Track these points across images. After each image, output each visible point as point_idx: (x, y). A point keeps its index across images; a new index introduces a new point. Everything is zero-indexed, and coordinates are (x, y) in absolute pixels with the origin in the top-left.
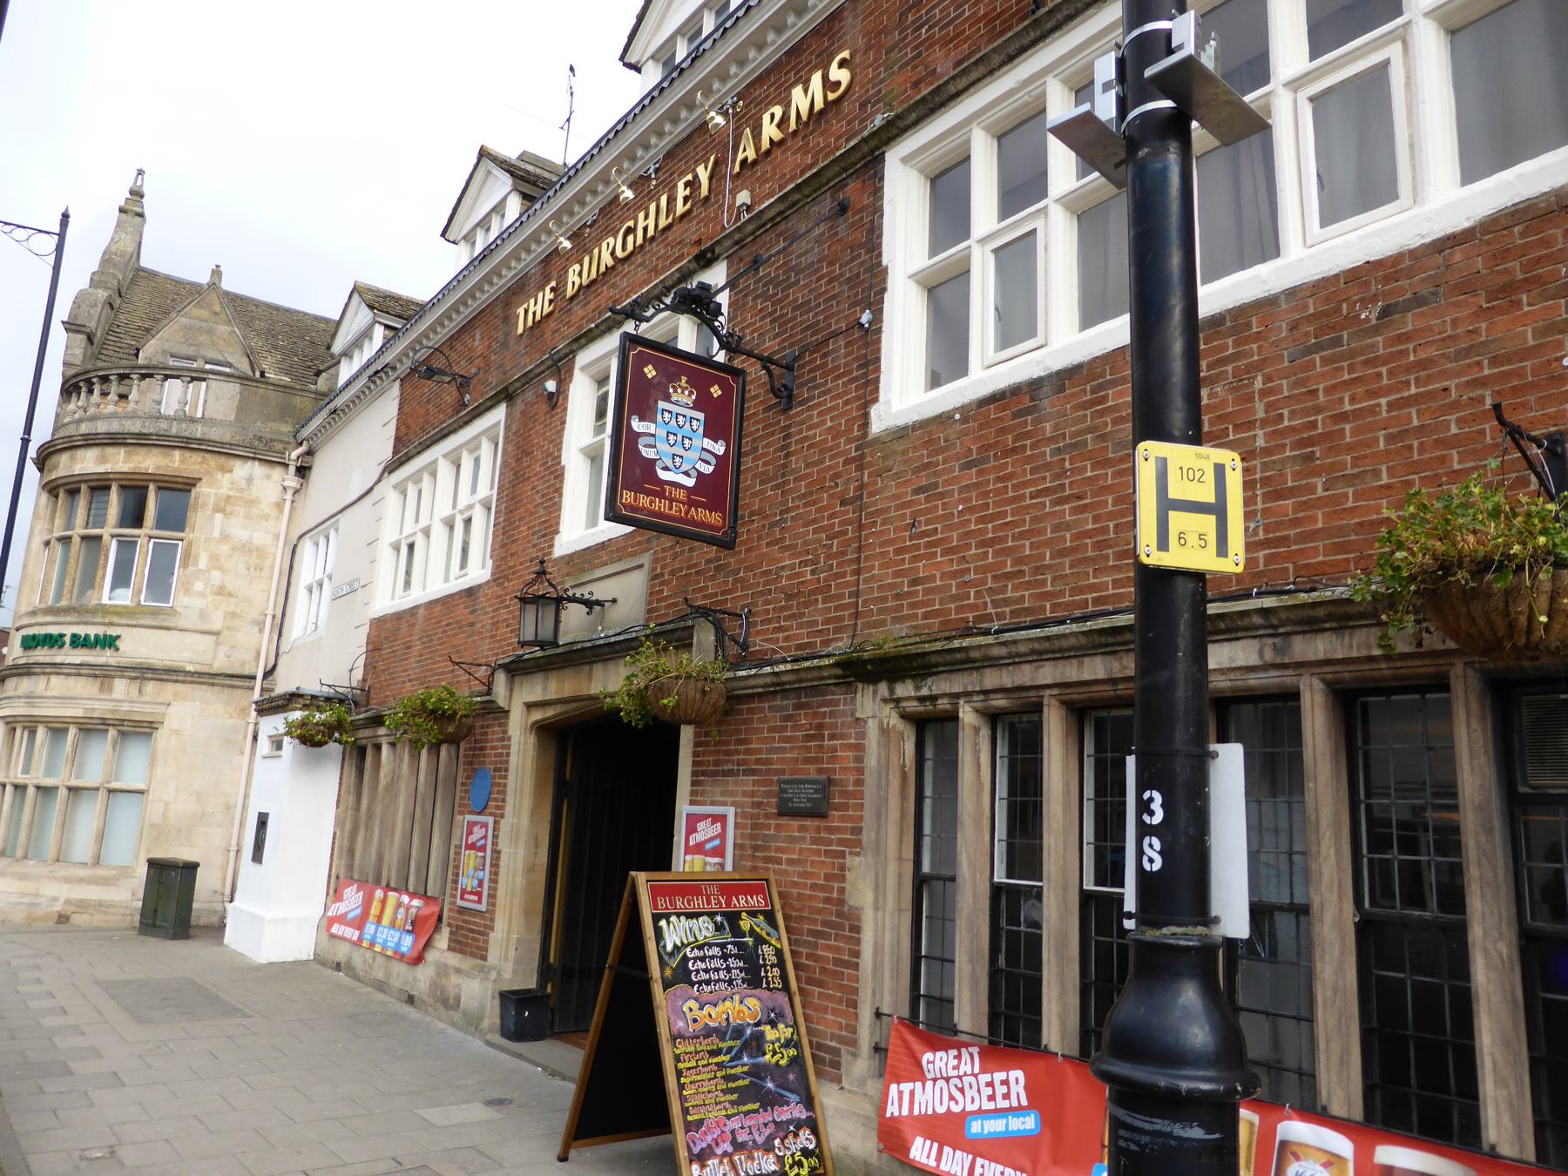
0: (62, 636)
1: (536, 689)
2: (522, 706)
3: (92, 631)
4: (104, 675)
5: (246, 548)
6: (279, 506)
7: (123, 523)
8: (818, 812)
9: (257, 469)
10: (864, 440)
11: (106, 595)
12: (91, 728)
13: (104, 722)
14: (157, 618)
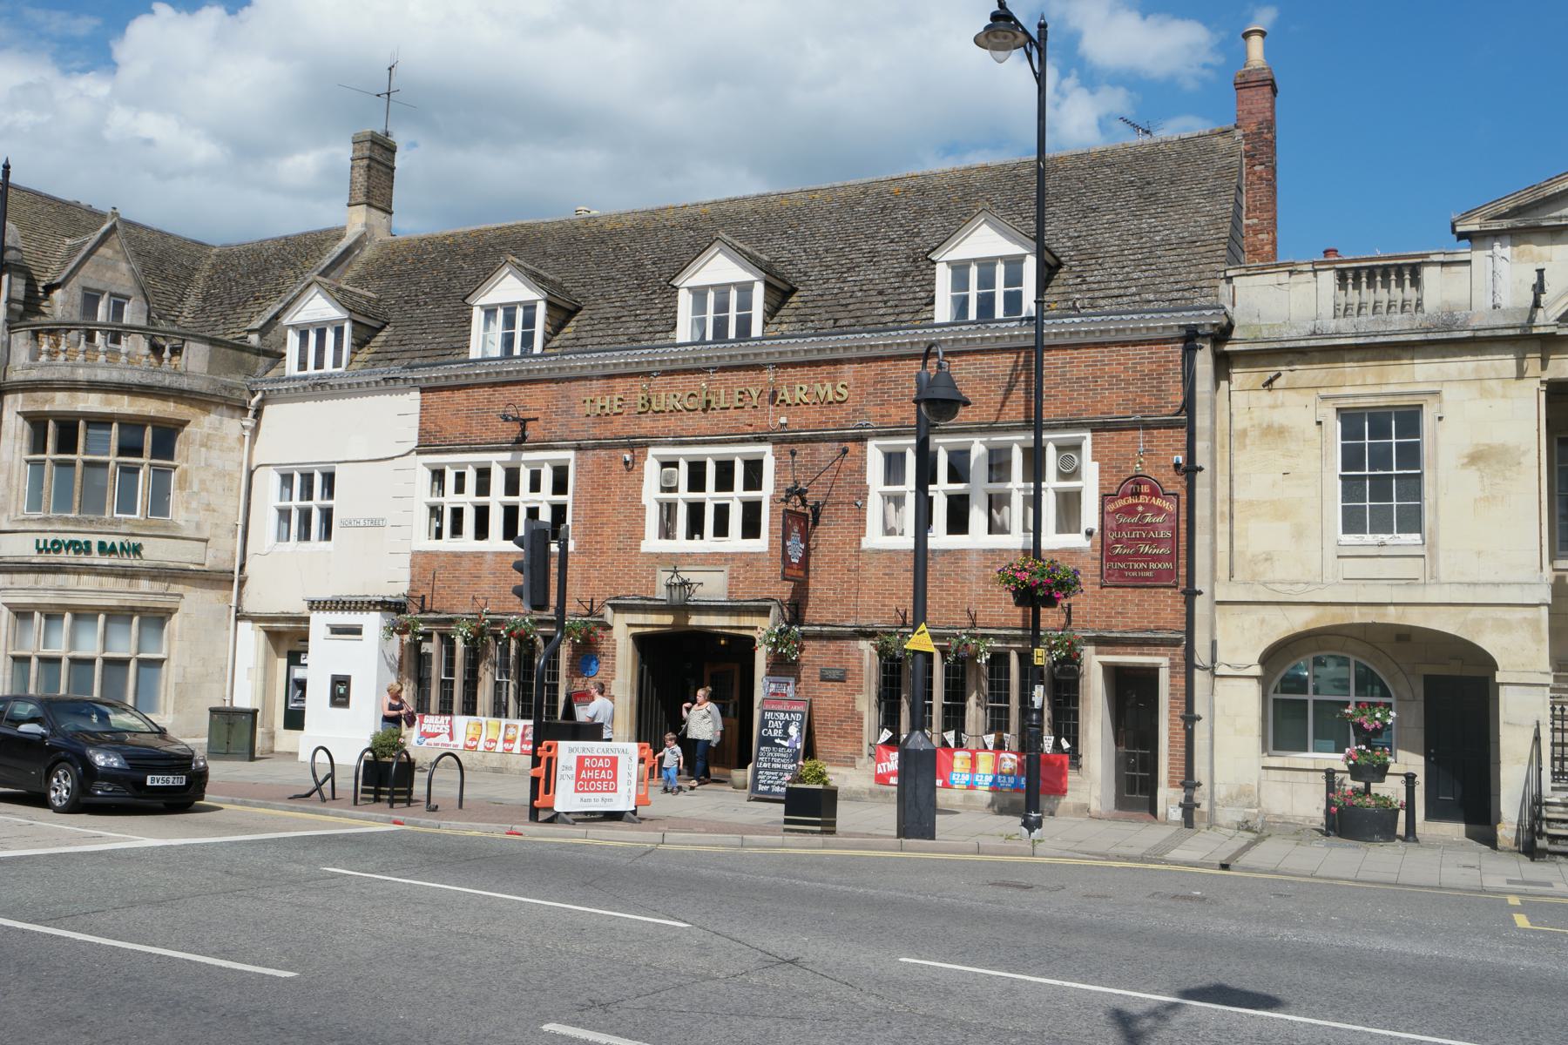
0: (88, 543)
8: (842, 680)
10: (859, 551)
13: (133, 610)
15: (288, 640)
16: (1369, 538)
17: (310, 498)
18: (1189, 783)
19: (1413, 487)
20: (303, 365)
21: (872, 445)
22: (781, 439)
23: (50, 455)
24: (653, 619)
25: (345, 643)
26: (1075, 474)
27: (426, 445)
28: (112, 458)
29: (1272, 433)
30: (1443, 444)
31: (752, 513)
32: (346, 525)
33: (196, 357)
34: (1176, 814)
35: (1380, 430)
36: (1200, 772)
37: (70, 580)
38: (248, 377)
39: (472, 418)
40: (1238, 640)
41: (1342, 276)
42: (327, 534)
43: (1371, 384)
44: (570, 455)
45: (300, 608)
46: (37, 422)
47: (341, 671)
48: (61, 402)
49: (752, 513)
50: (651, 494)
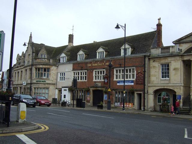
1: (93, 88)
2: (91, 89)
3: (43, 81)
4: (45, 84)
5: (54, 73)
6: (56, 70)
7: (44, 71)
9: (54, 67)
11: (44, 77)
12: (44, 88)
14: (49, 79)
15: (60, 91)
16: (164, 79)
17: (117, 73)
18: (144, 106)
19: (168, 73)
20: (62, 61)
21: (114, 69)
22: (136, 67)
23: (37, 72)
24: (94, 88)
25: (65, 91)
26: (134, 72)
27: (73, 70)
28: (43, 72)
29: (154, 67)
30: (172, 67)
31: (133, 75)
32: (66, 79)
33: (51, 61)
34: (143, 109)
35: (165, 66)
36: (146, 105)
37: (39, 85)
38: (57, 63)
39: (78, 67)
40: (151, 90)
41: (162, 49)
42: (64, 80)
43: (164, 61)
44: (86, 71)
45: (61, 88)
46: (36, 68)
47: (65, 94)
48: (38, 66)
49: (133, 75)
50: (94, 75)
